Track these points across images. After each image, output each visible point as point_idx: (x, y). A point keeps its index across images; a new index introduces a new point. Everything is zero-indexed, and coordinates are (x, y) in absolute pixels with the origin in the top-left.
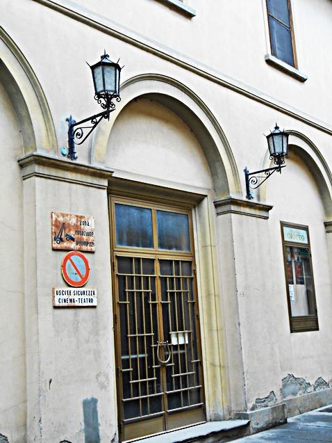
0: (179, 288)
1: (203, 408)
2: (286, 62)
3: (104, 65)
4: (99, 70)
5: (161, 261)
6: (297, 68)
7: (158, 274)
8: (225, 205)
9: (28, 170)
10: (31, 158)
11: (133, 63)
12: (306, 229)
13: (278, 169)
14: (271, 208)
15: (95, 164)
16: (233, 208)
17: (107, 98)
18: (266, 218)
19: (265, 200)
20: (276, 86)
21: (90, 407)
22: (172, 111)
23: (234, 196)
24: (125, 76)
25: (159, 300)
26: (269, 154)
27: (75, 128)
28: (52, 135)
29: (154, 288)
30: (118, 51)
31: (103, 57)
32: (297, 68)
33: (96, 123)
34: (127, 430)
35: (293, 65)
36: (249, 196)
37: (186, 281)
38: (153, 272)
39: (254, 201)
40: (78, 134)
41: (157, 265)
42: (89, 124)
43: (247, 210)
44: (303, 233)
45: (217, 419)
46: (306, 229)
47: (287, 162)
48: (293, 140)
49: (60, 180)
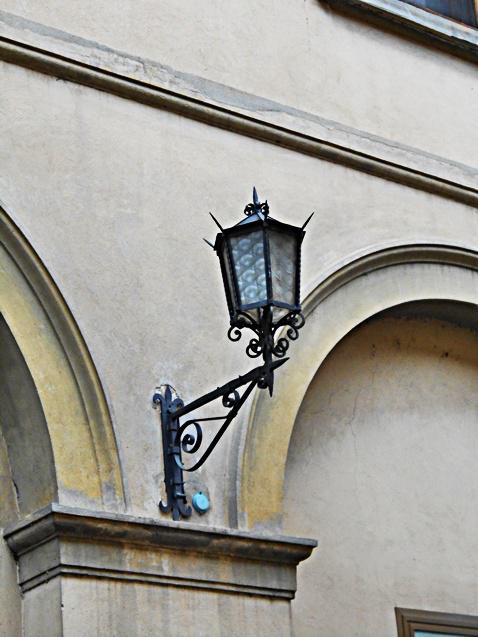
2: (447, 15)
3: (265, 233)
4: (239, 245)
9: (42, 560)
10: (48, 523)
11: (341, 220)
14: (304, 550)
16: (67, 554)
17: (266, 325)
18: (288, 595)
24: (317, 264)
27: (183, 420)
28: (106, 452)
30: (291, 187)
31: (253, 209)
33: (237, 404)
36: (176, 500)
40: (188, 440)
42: (217, 407)
43: (164, 564)
49: (150, 583)
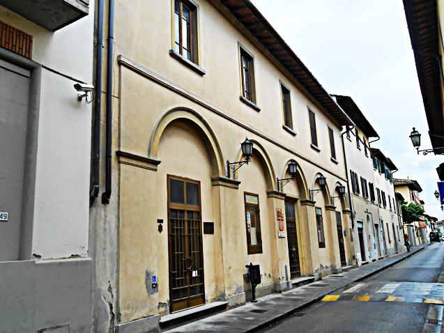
0: (181, 226)
1: (203, 296)
5: (188, 211)
6: (197, 64)
7: (186, 218)
8: (304, 202)
12: (257, 196)
13: (247, 162)
14: (159, 162)
15: (151, 158)
18: (156, 170)
19: (156, 155)
20: (284, 138)
21: (286, 267)
22: (189, 126)
23: (221, 176)
25: (186, 233)
26: (242, 153)
29: (184, 227)
32: (197, 64)
34: (175, 306)
35: (317, 146)
37: (184, 223)
38: (193, 218)
39: (231, 178)
41: (186, 214)
44: (256, 198)
45: (304, 276)
46: (257, 196)
47: (251, 159)
48: (255, 146)
